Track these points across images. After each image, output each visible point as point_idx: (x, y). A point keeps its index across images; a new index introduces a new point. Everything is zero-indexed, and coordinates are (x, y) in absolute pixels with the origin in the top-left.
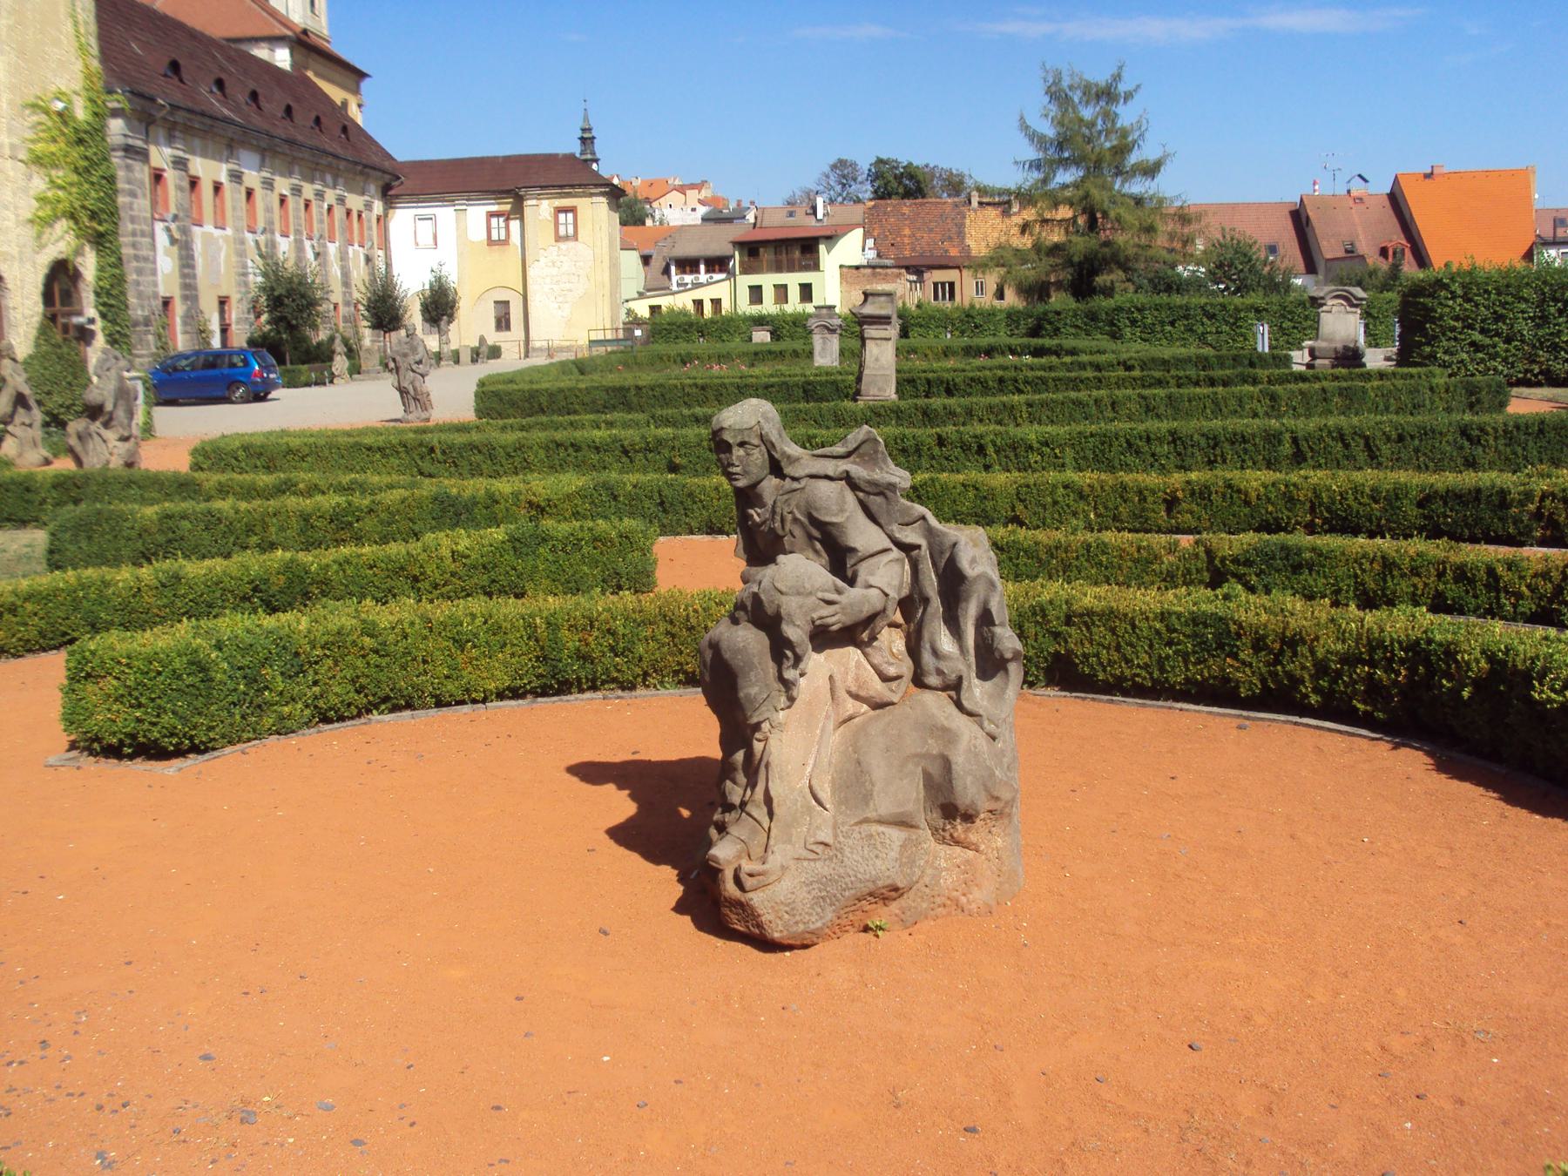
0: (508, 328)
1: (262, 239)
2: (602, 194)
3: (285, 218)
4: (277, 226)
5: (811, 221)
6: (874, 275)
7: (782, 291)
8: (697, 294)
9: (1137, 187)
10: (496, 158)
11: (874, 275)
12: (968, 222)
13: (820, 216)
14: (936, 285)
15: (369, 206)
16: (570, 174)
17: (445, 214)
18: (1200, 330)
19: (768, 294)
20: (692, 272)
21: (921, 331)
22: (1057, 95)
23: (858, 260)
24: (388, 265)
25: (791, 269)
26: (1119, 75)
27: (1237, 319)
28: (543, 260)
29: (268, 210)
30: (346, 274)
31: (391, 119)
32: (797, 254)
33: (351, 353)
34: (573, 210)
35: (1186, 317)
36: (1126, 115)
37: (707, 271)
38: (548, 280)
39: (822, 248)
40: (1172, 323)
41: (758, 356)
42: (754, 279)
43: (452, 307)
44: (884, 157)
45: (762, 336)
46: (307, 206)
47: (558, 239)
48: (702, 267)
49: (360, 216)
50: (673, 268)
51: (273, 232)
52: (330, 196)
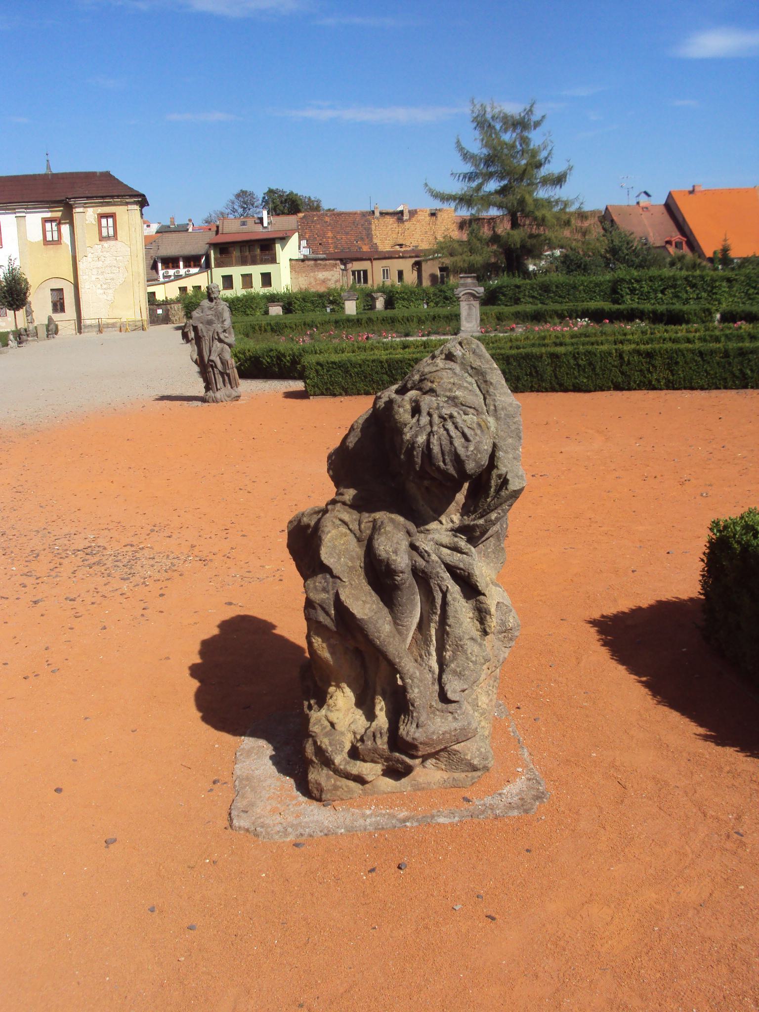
0: (62, 310)
5: (259, 228)
6: (316, 265)
7: (247, 279)
8: (182, 283)
9: (542, 193)
11: (316, 265)
12: (373, 227)
13: (265, 224)
14: (353, 272)
16: (106, 190)
18: (685, 296)
19: (237, 282)
20: (173, 268)
21: (405, 303)
22: (482, 123)
23: (297, 255)
25: (254, 262)
26: (531, 110)
27: (713, 288)
28: (89, 255)
32: (258, 251)
34: (112, 216)
35: (674, 286)
36: (536, 138)
38: (95, 272)
39: (278, 246)
40: (662, 292)
41: (276, 328)
42: (226, 271)
43: (25, 294)
45: (276, 310)
47: (102, 239)
48: (181, 264)
50: (160, 265)
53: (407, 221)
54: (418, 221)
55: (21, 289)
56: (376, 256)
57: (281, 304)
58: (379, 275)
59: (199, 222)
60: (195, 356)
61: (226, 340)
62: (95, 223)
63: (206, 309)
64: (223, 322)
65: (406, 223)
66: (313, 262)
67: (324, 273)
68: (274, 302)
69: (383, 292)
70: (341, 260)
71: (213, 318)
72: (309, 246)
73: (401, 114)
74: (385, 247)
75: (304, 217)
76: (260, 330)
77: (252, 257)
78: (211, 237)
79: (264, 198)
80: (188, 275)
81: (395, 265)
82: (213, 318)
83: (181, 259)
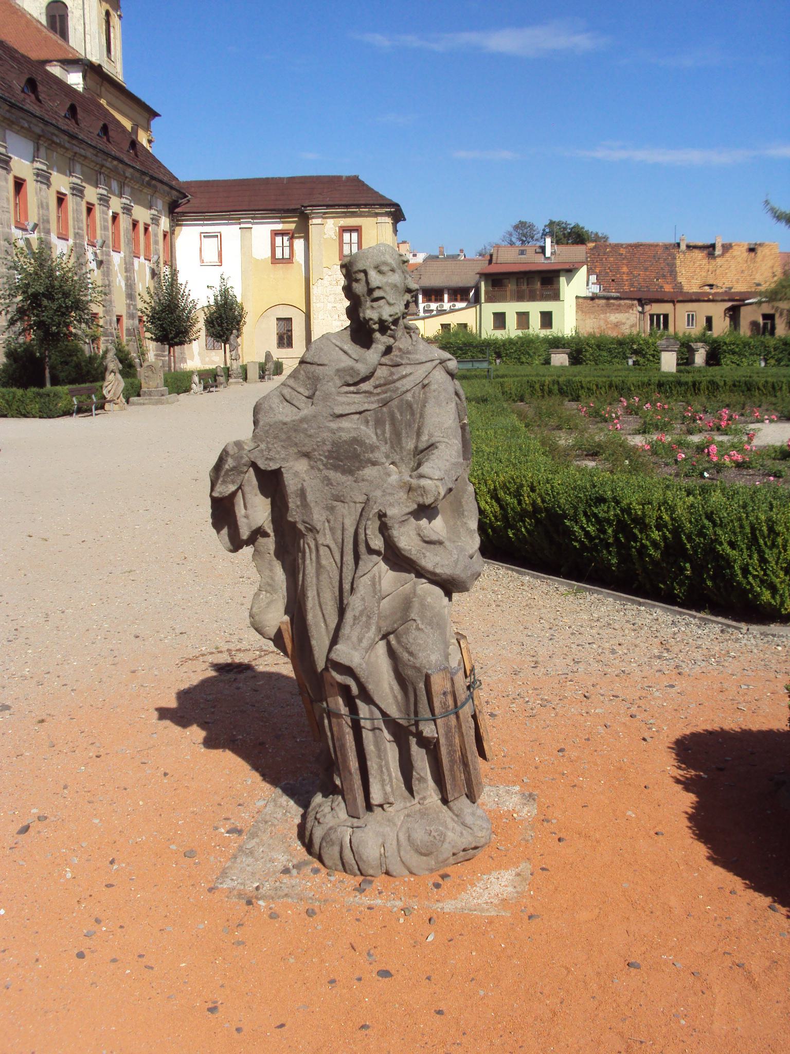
0: (290, 345)
1: (34, 237)
2: (387, 214)
3: (62, 220)
4: (53, 226)
5: (540, 259)
6: (608, 305)
7: (523, 318)
8: (445, 319)
10: (280, 179)
12: (678, 262)
13: (548, 254)
14: (652, 316)
15: (155, 220)
17: (230, 232)
19: (511, 321)
20: (436, 301)
23: (585, 293)
24: (174, 273)
25: (532, 298)
28: (326, 278)
29: (42, 206)
30: (130, 285)
31: (182, 149)
32: (538, 285)
33: (128, 368)
34: (357, 229)
37: (449, 301)
39: (563, 280)
42: (499, 307)
43: (238, 323)
44: (556, 219)
45: (560, 359)
46: (90, 210)
48: (446, 297)
49: (146, 229)
50: (420, 297)
51: (48, 232)
52: (116, 204)
53: (719, 256)
54: (734, 257)
55: (235, 318)
56: (680, 298)
57: (568, 350)
58: (684, 321)
59: (471, 254)
60: (277, 617)
61: (430, 560)
62: (336, 238)
63: (331, 386)
64: (422, 453)
65: (718, 260)
66: (604, 301)
67: (617, 315)
68: (558, 348)
69: (704, 342)
70: (640, 300)
71: (369, 434)
72: (599, 282)
73: (694, 157)
74: (691, 286)
75: (595, 247)
76: (542, 390)
77: (530, 291)
78: (484, 267)
79: (544, 230)
80: (452, 311)
81: (703, 310)
82: (369, 434)
83: (446, 292)
